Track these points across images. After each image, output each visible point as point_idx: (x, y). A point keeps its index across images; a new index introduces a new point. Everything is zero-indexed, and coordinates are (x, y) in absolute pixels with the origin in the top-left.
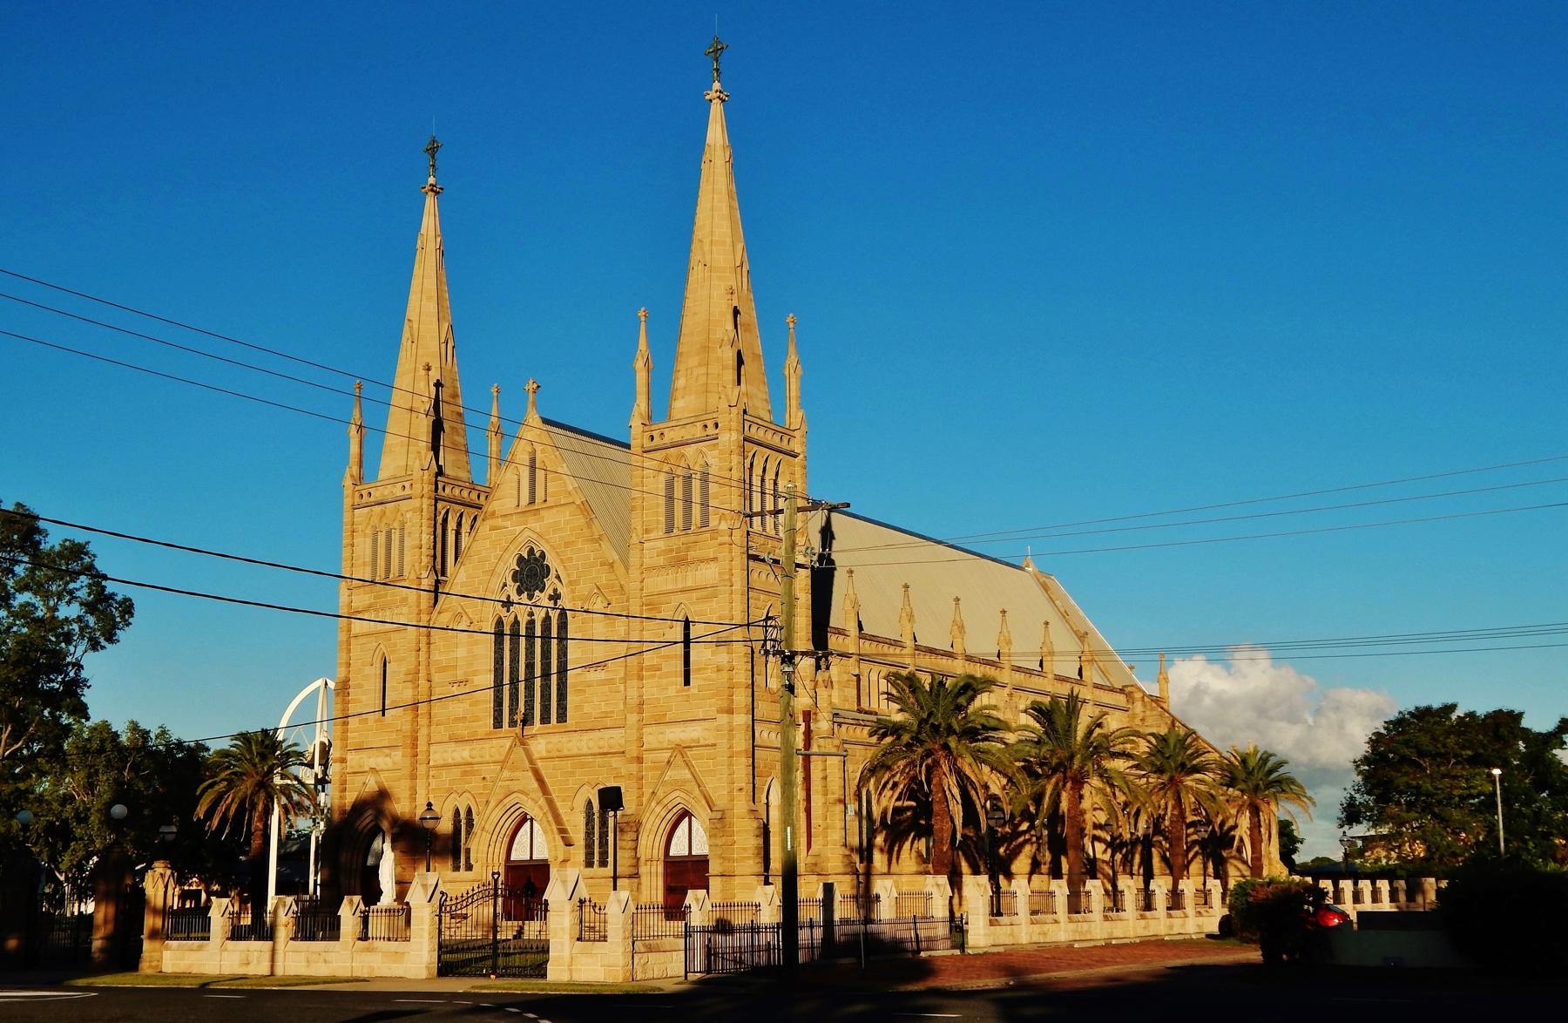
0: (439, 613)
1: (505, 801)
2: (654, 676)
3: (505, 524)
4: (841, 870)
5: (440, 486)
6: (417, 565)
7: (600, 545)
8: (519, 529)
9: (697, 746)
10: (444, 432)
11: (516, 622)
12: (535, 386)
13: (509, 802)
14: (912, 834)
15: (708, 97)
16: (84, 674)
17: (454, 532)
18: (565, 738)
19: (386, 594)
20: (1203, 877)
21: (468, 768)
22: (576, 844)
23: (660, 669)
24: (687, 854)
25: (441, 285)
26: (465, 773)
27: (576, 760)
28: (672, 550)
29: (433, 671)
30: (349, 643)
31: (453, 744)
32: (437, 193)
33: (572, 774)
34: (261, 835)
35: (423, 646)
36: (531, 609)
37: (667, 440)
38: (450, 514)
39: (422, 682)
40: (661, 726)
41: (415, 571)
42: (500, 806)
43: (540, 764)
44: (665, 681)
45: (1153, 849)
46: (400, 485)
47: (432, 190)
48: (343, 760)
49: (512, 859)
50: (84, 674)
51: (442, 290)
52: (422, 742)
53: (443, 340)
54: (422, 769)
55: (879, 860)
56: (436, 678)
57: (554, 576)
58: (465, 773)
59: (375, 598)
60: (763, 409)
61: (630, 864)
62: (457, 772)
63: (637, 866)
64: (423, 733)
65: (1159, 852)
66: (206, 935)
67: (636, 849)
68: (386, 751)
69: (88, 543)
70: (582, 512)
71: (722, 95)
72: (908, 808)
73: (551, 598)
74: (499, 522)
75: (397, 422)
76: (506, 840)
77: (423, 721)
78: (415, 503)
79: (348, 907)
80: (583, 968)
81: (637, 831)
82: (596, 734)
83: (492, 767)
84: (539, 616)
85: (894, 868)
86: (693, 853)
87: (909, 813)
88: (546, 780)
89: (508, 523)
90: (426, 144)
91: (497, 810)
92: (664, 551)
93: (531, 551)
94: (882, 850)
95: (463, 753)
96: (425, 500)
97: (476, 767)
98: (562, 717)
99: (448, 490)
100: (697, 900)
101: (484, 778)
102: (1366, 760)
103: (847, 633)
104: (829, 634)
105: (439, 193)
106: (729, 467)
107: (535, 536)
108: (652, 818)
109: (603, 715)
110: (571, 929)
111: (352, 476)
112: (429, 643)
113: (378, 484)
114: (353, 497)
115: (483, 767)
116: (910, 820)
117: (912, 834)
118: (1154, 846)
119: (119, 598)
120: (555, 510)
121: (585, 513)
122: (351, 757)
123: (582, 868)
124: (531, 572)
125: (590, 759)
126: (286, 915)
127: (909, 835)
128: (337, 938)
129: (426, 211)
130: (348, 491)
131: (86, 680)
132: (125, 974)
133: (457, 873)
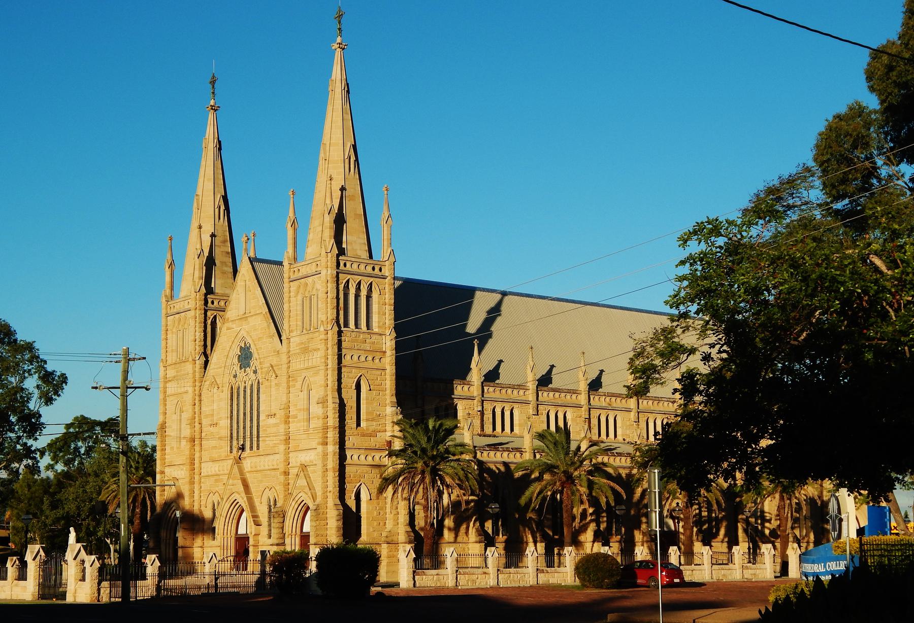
1: (230, 498)
4: (404, 541)
5: (210, 301)
6: (193, 351)
7: (273, 339)
8: (239, 329)
9: (312, 465)
10: (215, 265)
12: (246, 238)
13: (232, 499)
14: (474, 518)
15: (333, 48)
16: (42, 420)
17: (365, 296)
19: (181, 370)
20: (747, 543)
21: (216, 477)
22: (263, 524)
23: (297, 417)
25: (217, 170)
26: (217, 481)
28: (302, 343)
29: (202, 417)
30: (165, 400)
31: (211, 463)
32: (215, 110)
34: (140, 517)
35: (197, 402)
36: (247, 378)
37: (300, 274)
38: (350, 283)
39: (197, 424)
40: (298, 453)
41: (192, 356)
42: (228, 501)
43: (248, 476)
45: (739, 524)
46: (186, 302)
47: (212, 109)
48: (162, 472)
49: (239, 533)
50: (42, 420)
51: (217, 173)
52: (197, 461)
53: (346, 157)
54: (197, 477)
55: (447, 535)
56: (204, 422)
58: (217, 481)
59: (177, 372)
60: (360, 249)
61: (278, 537)
62: (213, 479)
63: (284, 538)
64: (197, 455)
65: (742, 525)
67: (282, 528)
69: (35, 342)
70: (265, 319)
71: (341, 46)
72: (472, 501)
75: (316, 224)
76: (235, 521)
77: (197, 448)
78: (192, 313)
79: (403, 553)
80: (79, 595)
81: (284, 516)
82: (271, 457)
85: (459, 539)
87: (472, 504)
88: (251, 485)
89: (234, 326)
90: (209, 80)
91: (227, 503)
92: (299, 344)
94: (450, 529)
96: (197, 311)
98: (258, 448)
99: (216, 303)
100: (568, 551)
103: (472, 383)
104: (455, 386)
105: (217, 110)
106: (326, 291)
108: (291, 509)
110: (75, 575)
111: (166, 296)
112: (200, 400)
113: (179, 300)
114: (167, 309)
116: (473, 509)
117: (474, 518)
118: (739, 522)
119: (58, 374)
120: (254, 317)
121: (267, 319)
122: (167, 470)
123: (266, 539)
124: (245, 357)
125: (268, 472)
126: (12, 566)
127: (472, 518)
128: (26, 580)
129: (209, 123)
130: (164, 306)
131: (43, 424)
133: (214, 541)
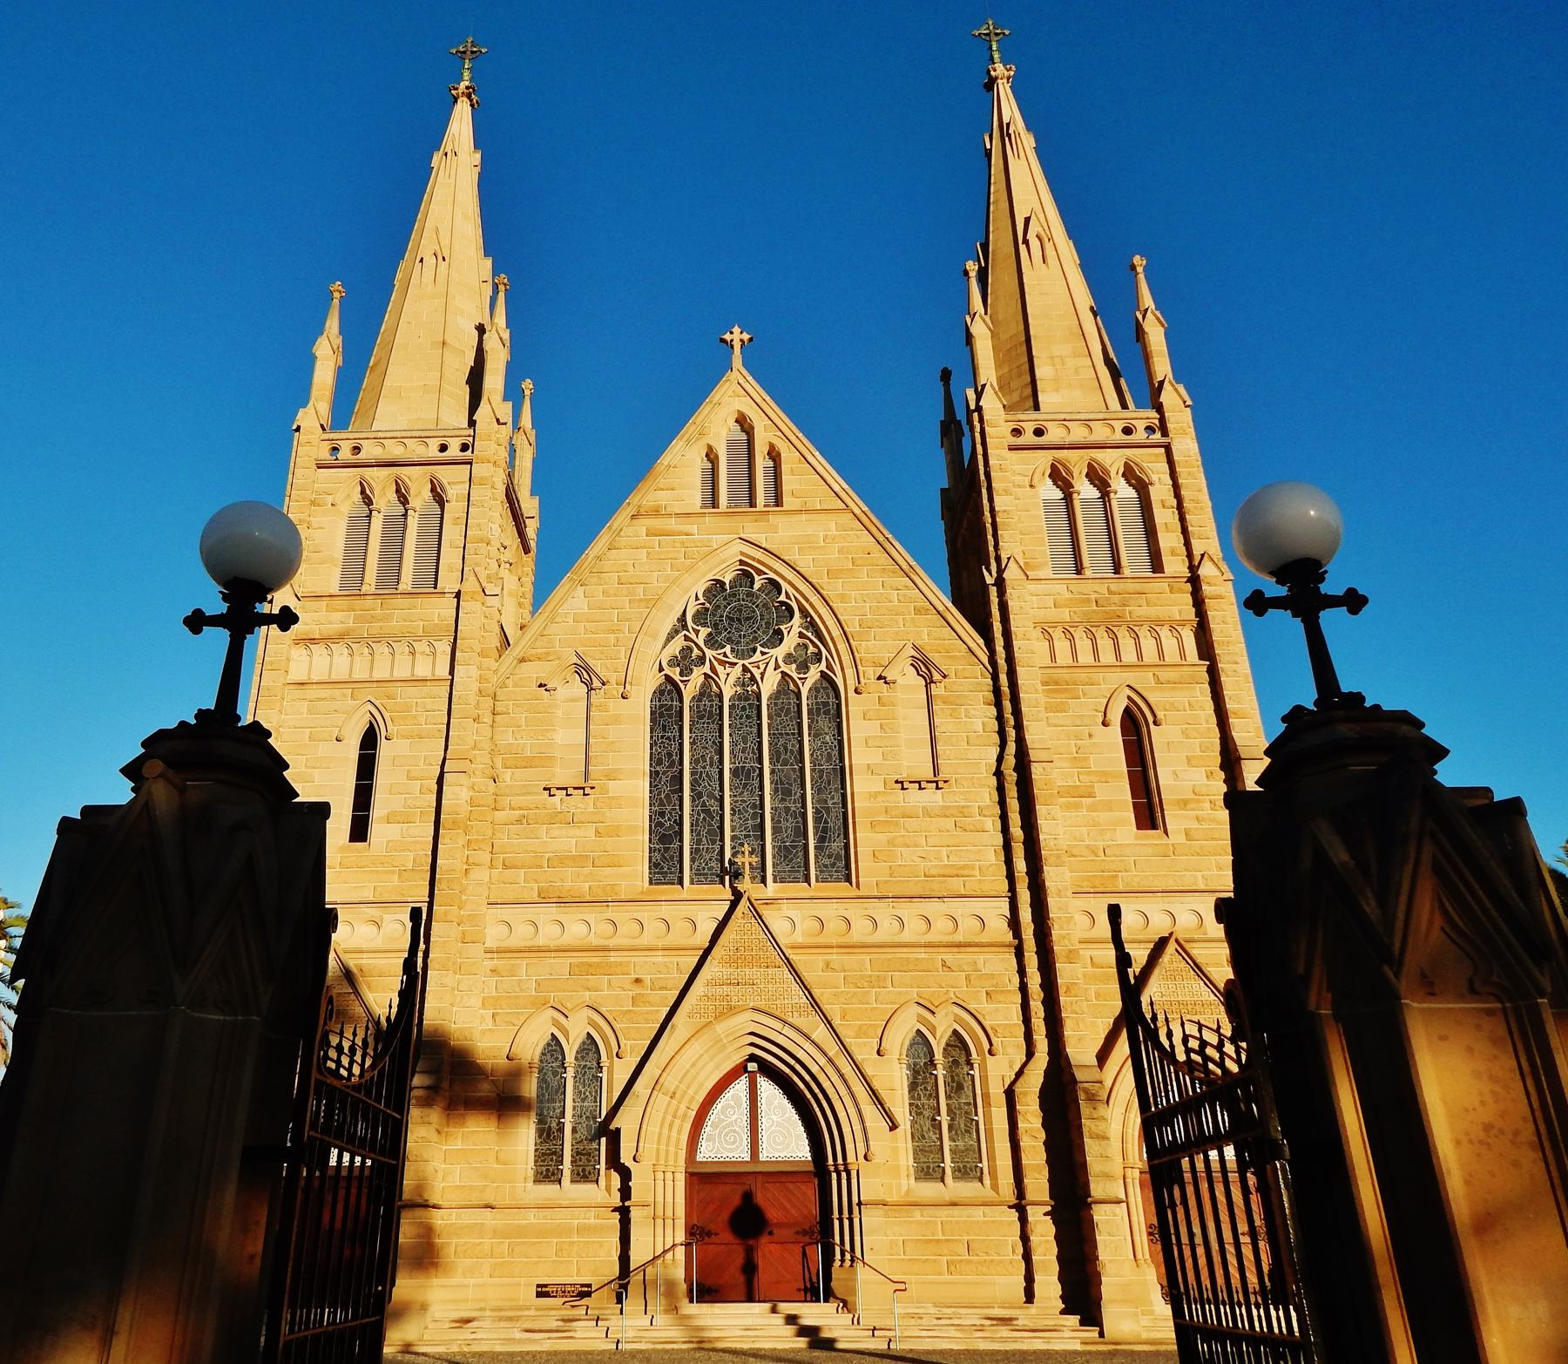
0: (522, 660)
2: (1077, 806)
3: (686, 528)
11: (709, 693)
12: (746, 337)
18: (854, 911)
24: (748, 1159)
27: (889, 955)
33: (879, 982)
44: (1103, 816)
56: (507, 776)
57: (798, 624)
58: (588, 969)
62: (562, 964)
66: (540, 1289)
68: (373, 912)
73: (789, 658)
74: (673, 524)
83: (660, 959)
84: (769, 686)
86: (763, 1156)
89: (694, 529)
93: (745, 576)
95: (577, 927)
97: (614, 958)
101: (638, 981)
102: (499, 1117)
107: (758, 554)
109: (947, 872)
115: (637, 958)
125: (922, 954)
132: (1473, 1301)
